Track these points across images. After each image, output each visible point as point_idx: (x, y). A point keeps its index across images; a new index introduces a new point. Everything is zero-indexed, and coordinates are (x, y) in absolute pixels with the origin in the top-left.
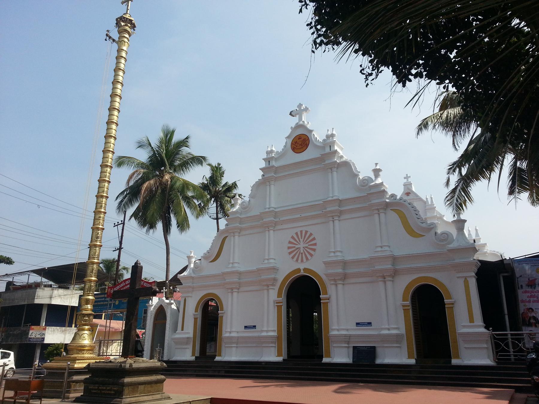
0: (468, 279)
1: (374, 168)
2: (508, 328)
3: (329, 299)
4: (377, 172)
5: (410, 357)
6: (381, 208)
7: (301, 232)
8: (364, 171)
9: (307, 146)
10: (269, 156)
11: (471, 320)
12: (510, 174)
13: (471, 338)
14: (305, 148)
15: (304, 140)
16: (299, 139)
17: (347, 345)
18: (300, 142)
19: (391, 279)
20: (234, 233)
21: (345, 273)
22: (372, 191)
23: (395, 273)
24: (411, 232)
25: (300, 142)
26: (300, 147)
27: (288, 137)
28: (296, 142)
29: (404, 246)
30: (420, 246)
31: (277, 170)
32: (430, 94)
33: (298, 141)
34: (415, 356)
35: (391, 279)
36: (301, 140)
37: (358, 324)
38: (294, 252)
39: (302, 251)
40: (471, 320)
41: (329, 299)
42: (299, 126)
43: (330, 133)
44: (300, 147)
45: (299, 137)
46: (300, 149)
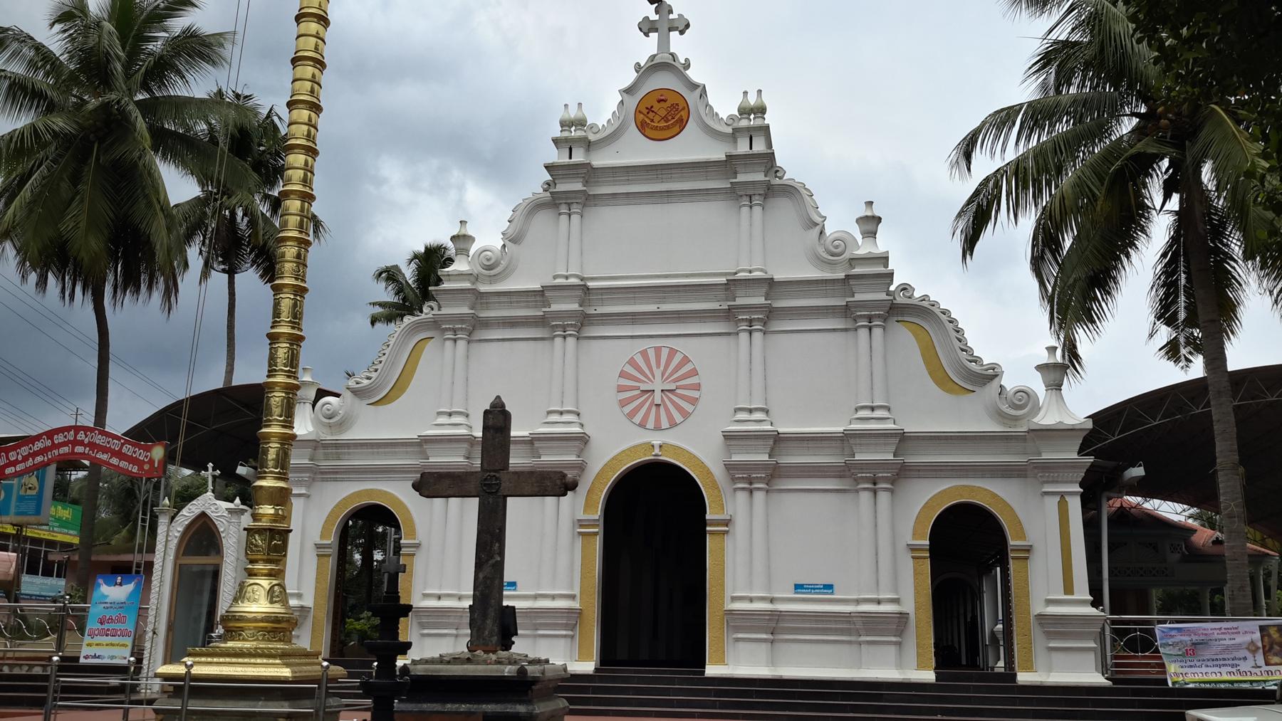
0: (1067, 498)
1: (864, 212)
2: (187, 688)
3: (1028, 551)
4: (870, 224)
5: (921, 666)
6: (879, 316)
7: (658, 350)
8: (840, 220)
9: (682, 124)
10: (566, 134)
11: (1069, 589)
12: (1164, 255)
13: (1057, 627)
14: (677, 129)
15: (675, 107)
16: (659, 101)
17: (770, 636)
18: (662, 105)
19: (889, 486)
20: (455, 331)
21: (771, 464)
22: (858, 270)
23: (900, 474)
24: (943, 381)
25: (662, 105)
26: (663, 124)
27: (628, 91)
28: (650, 109)
29: (932, 413)
30: (970, 416)
31: (588, 173)
32: (1227, 345)
33: (657, 107)
34: (934, 664)
35: (889, 486)
36: (662, 104)
37: (798, 587)
38: (636, 398)
39: (658, 401)
40: (1069, 589)
41: (1028, 551)
42: (656, 66)
43: (752, 100)
44: (663, 124)
45: (661, 96)
46: (662, 129)
